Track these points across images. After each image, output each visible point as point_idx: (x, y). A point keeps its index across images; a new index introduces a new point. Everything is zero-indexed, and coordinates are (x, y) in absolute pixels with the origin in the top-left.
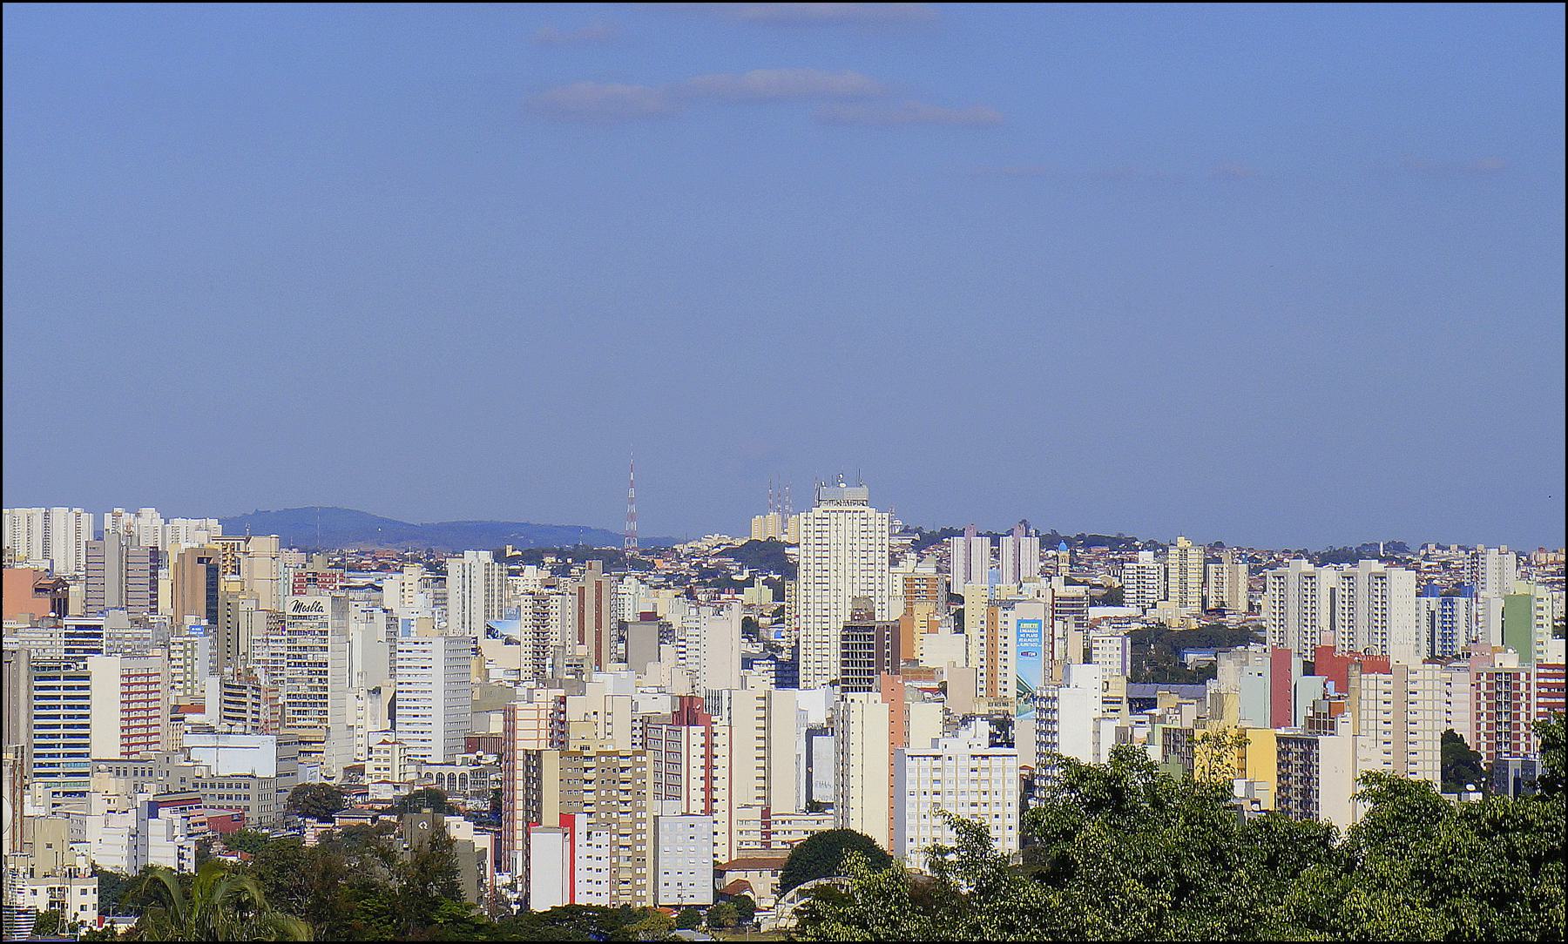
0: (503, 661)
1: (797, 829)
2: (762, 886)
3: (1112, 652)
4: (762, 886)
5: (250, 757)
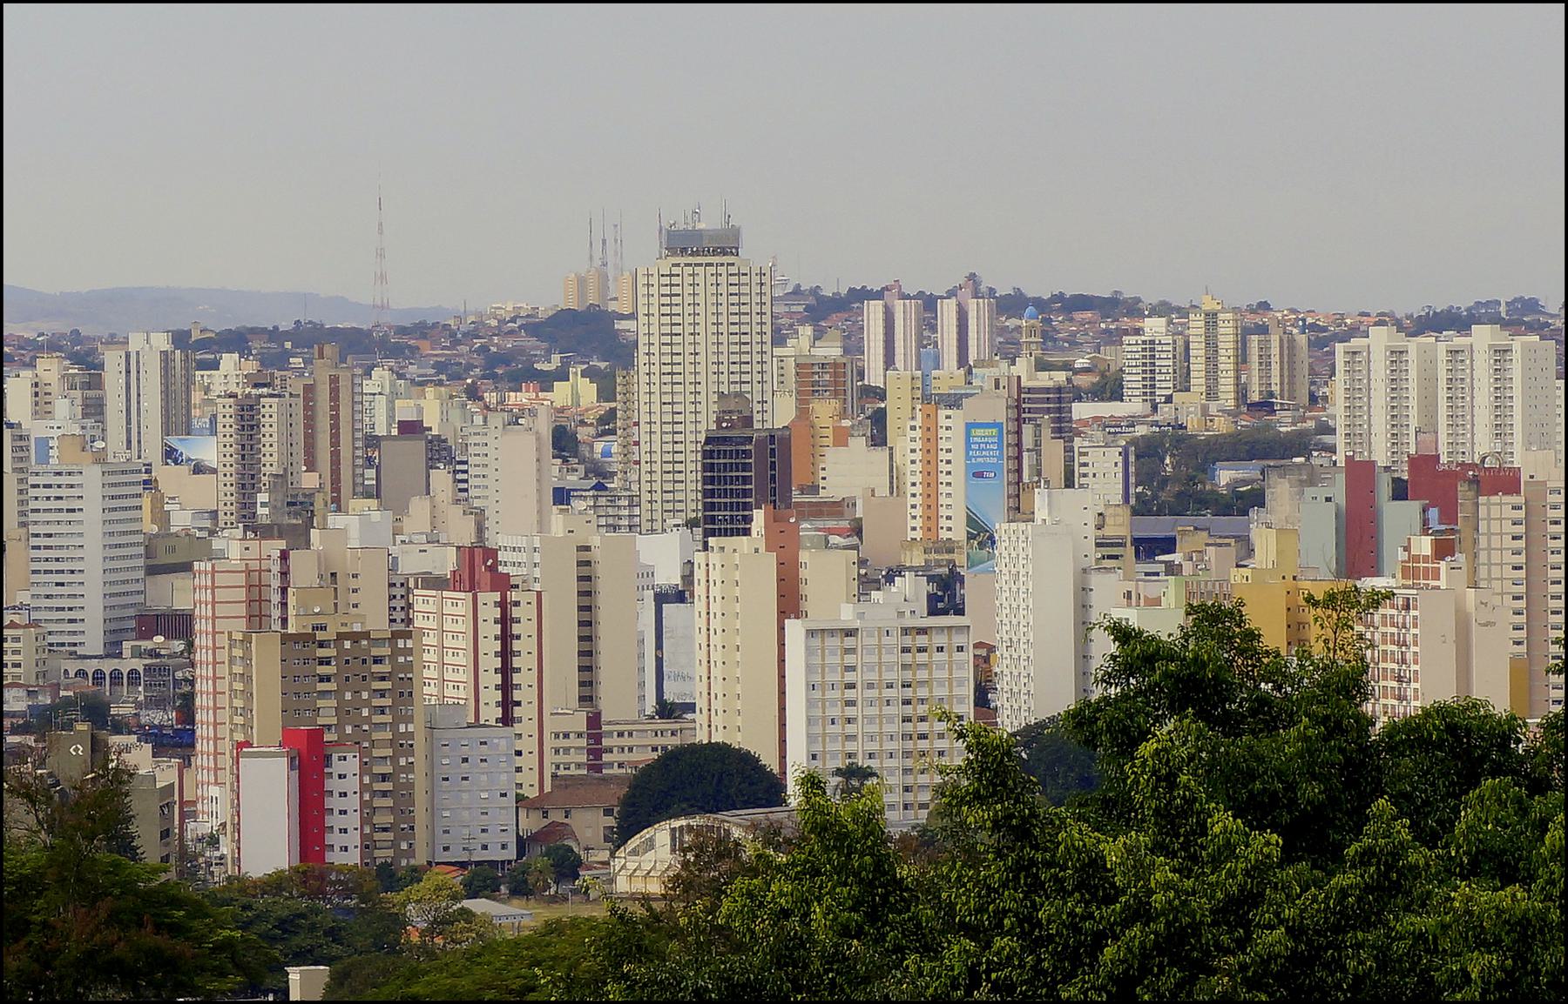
0: (190, 499)
1: (635, 749)
2: (589, 826)
3: (1106, 472)
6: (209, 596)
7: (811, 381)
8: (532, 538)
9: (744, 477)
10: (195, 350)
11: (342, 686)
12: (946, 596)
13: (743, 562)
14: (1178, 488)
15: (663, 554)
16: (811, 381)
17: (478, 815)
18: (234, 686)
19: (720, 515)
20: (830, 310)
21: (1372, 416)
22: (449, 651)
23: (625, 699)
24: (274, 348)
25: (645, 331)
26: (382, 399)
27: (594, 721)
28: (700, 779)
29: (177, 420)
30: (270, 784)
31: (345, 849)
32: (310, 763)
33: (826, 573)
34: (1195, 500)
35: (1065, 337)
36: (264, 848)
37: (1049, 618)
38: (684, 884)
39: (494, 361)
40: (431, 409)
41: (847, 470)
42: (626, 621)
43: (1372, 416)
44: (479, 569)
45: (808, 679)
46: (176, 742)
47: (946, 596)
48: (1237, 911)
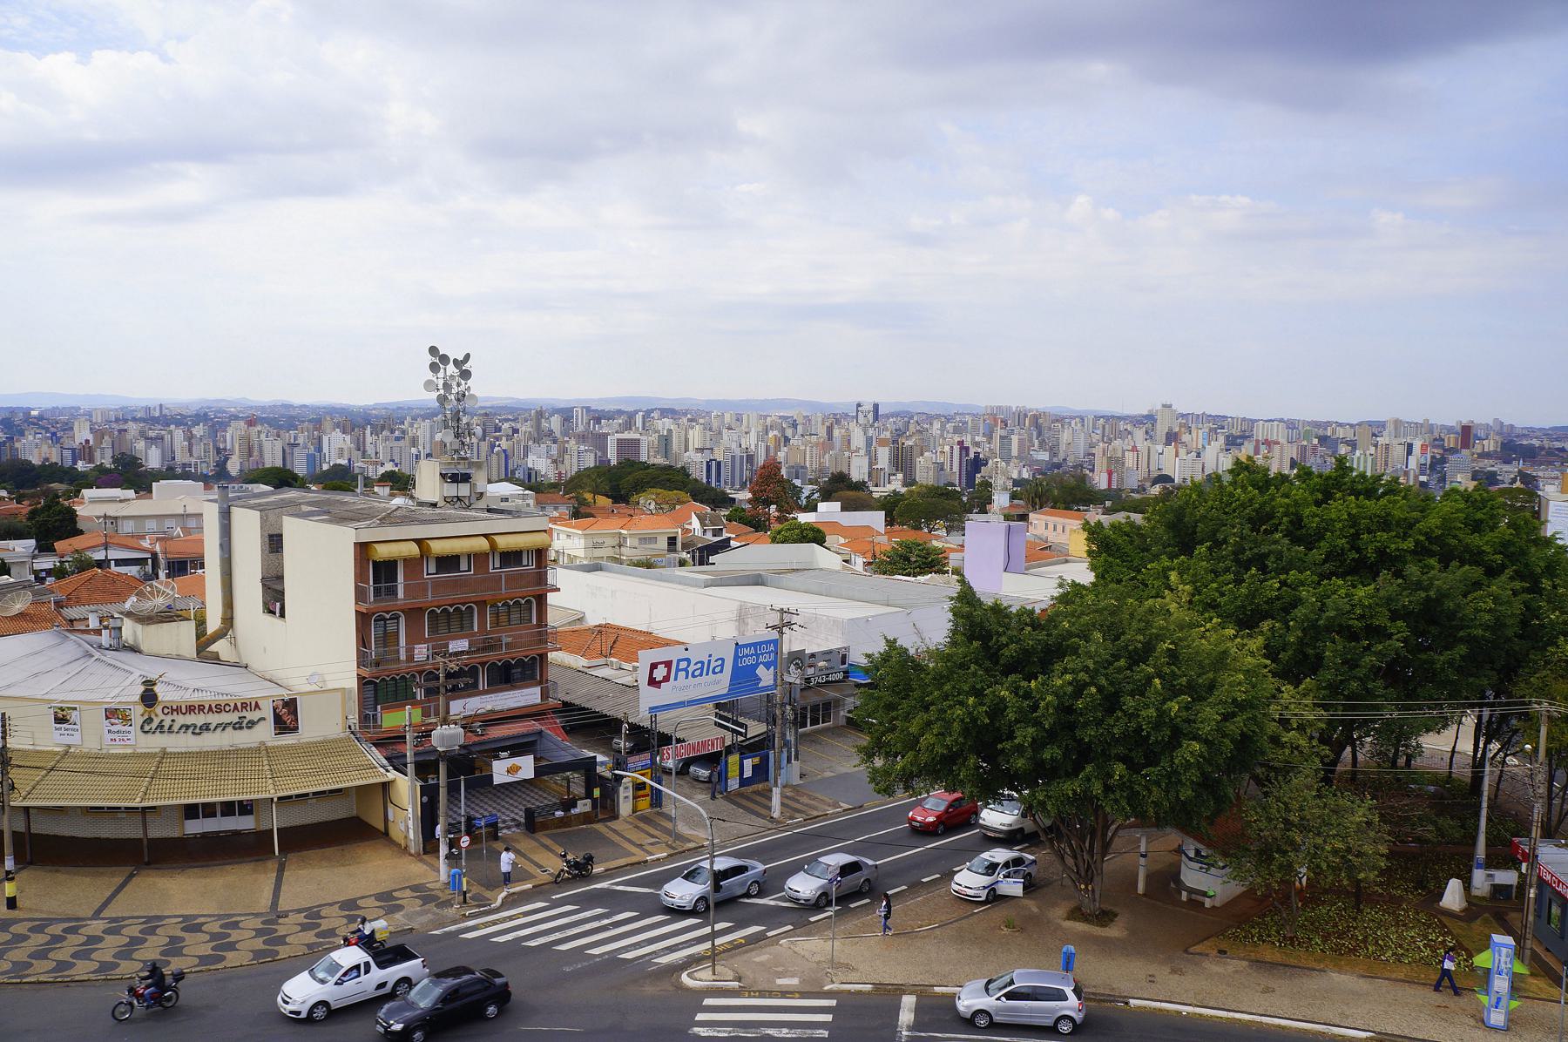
0: (1096, 438)
1: (1155, 474)
2: (1148, 484)
3: (1222, 439)
4: (1148, 484)
5: (1044, 456)
6: (1098, 451)
7: (1181, 425)
8: (1142, 445)
9: (1172, 438)
10: (1097, 418)
11: (1115, 464)
12: (1198, 455)
13: (1171, 449)
14: (1232, 442)
15: (1160, 448)
16: (1181, 425)
17: (1132, 482)
18: (1100, 463)
19: (1168, 443)
20: (1183, 416)
21: (1260, 433)
22: (1130, 460)
23: (1153, 467)
24: (1108, 418)
25: (1159, 417)
26: (1122, 426)
27: (1453, 751)
28: (1164, 479)
29: (1094, 427)
30: (1105, 476)
31: (1114, 486)
32: (1110, 474)
33: (1182, 451)
34: (1234, 444)
35: (1217, 423)
36: (1104, 485)
37: (1217, 459)
38: (601, 777)
39: (1137, 421)
40: (1129, 427)
41: (1185, 438)
42: (1154, 457)
43: (1260, 433)
44: (1134, 449)
45: (1179, 467)
46: (1092, 470)
47: (1198, 455)
48: (1251, 500)
